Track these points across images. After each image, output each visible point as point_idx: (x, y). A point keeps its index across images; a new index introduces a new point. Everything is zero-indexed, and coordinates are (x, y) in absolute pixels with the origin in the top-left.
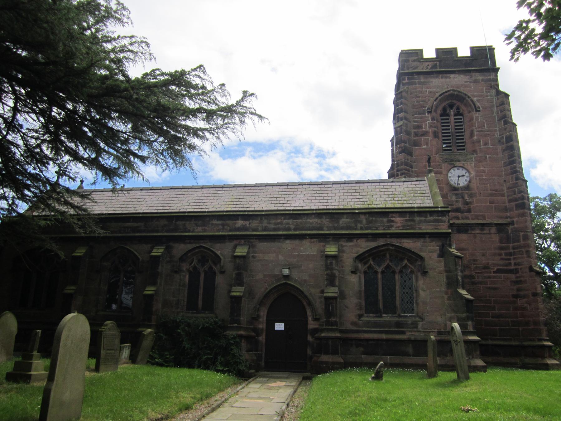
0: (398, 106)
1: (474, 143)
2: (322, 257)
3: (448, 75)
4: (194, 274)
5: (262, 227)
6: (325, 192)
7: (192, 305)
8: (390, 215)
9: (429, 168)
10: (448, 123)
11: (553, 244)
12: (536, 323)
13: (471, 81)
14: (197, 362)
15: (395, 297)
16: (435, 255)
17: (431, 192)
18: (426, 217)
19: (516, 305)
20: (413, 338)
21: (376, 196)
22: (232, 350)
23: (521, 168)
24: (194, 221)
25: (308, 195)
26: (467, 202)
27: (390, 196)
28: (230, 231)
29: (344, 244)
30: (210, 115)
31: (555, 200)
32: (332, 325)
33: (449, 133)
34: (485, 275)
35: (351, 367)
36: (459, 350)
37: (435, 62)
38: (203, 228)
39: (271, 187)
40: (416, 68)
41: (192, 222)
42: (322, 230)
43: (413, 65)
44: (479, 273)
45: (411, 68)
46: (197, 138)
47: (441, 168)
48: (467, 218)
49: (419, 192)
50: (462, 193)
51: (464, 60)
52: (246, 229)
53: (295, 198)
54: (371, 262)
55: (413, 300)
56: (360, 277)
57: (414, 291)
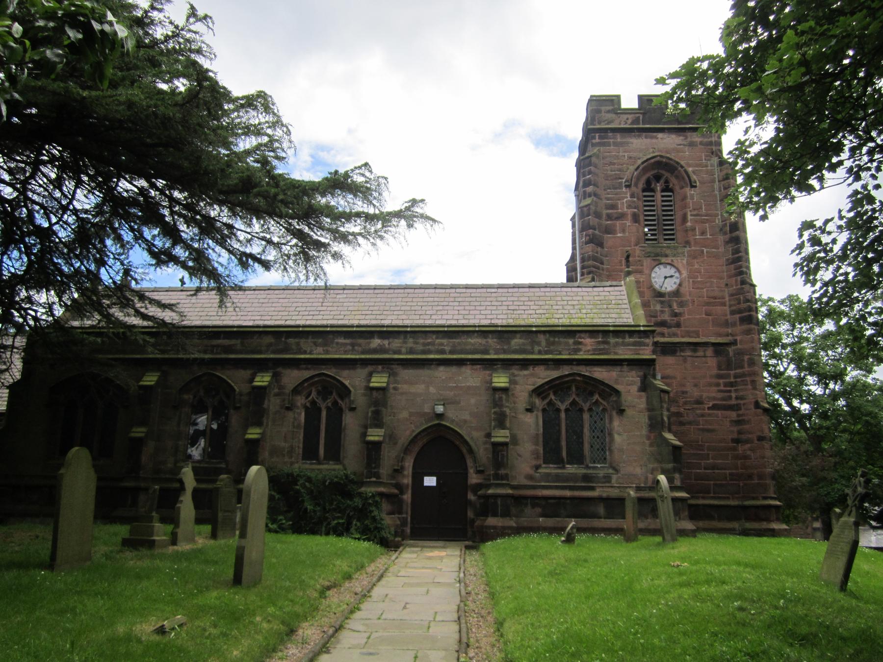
0: (584, 176)
1: (687, 231)
2: (487, 390)
3: (655, 134)
4: (313, 412)
5: (407, 348)
6: (488, 299)
7: (310, 453)
10: (653, 201)
12: (761, 477)
13: (685, 143)
14: (324, 529)
15: (582, 443)
16: (634, 389)
17: (630, 302)
18: (624, 338)
20: (605, 495)
21: (557, 307)
22: (371, 512)
23: (748, 268)
24: (313, 338)
25: (465, 304)
26: (676, 313)
27: (576, 307)
28: (363, 353)
29: (516, 372)
30: (369, 218)
33: (654, 215)
34: (698, 412)
35: (526, 533)
36: (665, 509)
37: (637, 115)
38: (325, 348)
39: (412, 291)
41: (309, 341)
42: (489, 354)
44: (689, 409)
45: (604, 121)
46: (345, 243)
47: (642, 265)
48: (675, 335)
49: (613, 302)
50: (669, 301)
52: (385, 351)
53: (447, 308)
55: (605, 447)
57: (607, 435)
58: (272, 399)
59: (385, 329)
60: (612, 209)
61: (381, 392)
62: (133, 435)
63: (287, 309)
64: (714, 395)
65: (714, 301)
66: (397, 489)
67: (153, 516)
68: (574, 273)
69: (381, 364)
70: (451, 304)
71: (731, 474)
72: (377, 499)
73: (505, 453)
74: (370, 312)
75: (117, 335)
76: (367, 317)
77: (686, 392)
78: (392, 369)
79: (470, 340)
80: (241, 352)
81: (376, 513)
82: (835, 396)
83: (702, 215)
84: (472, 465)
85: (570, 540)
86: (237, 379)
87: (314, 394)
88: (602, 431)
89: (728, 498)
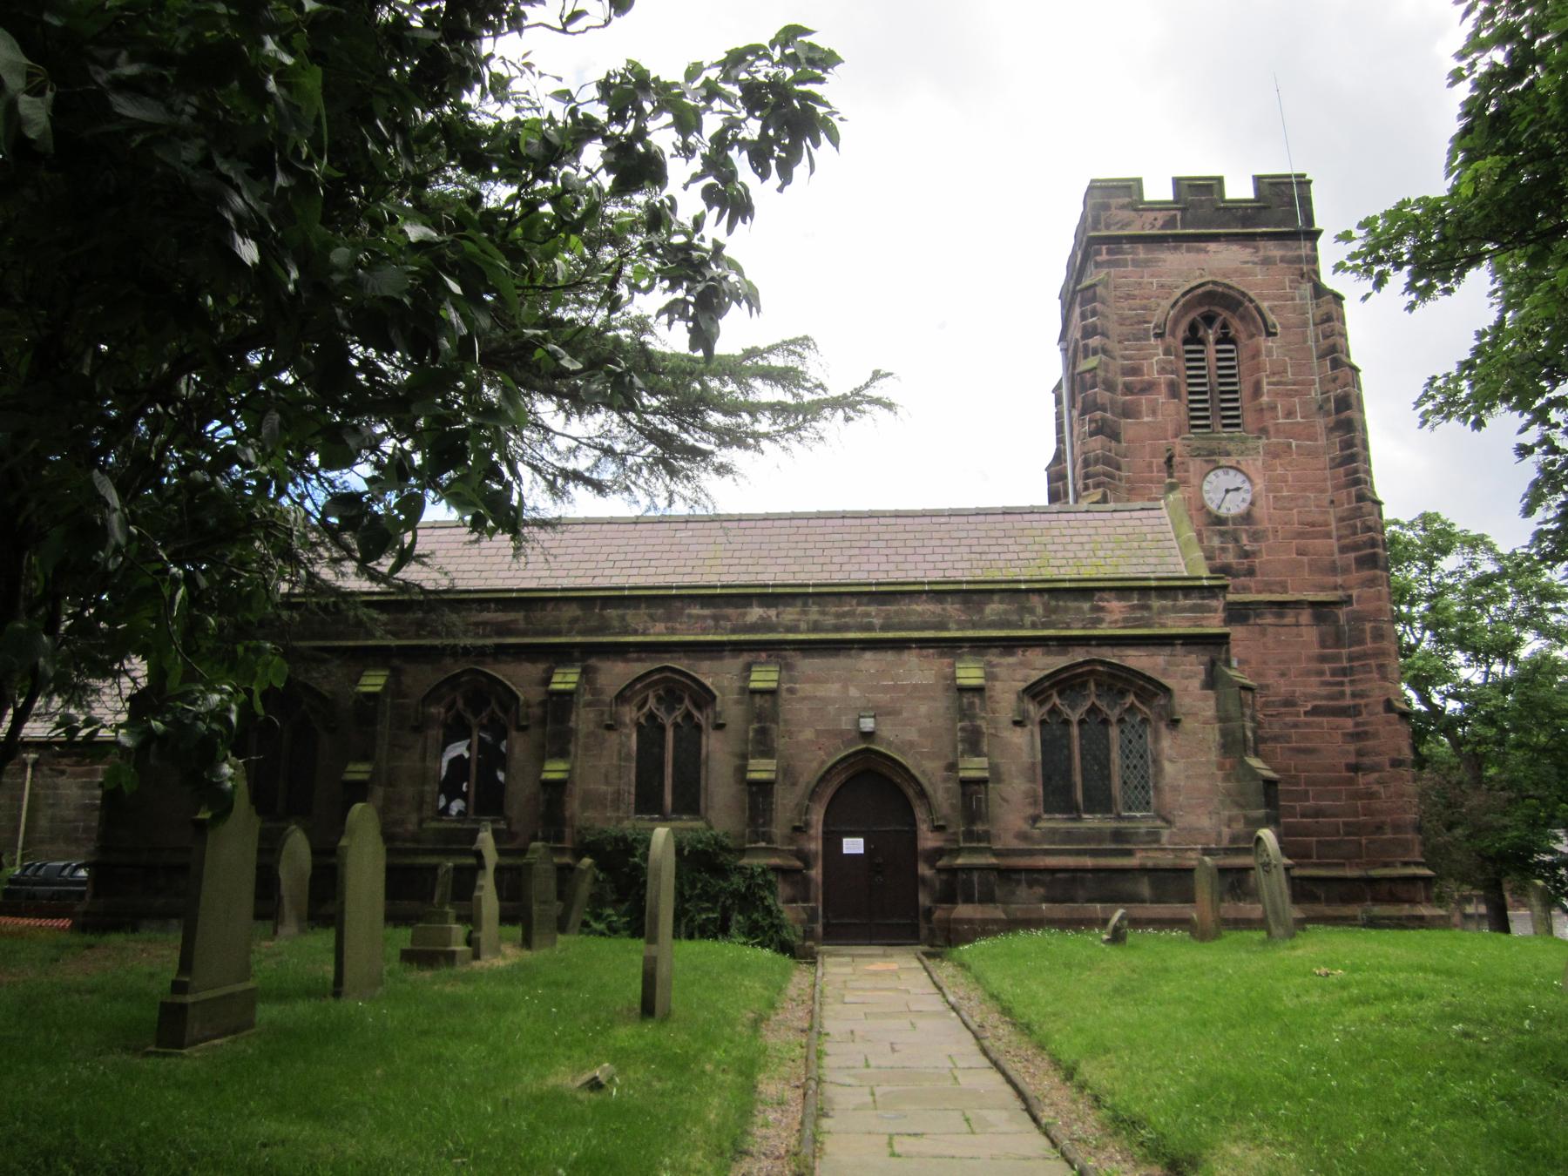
1: (1262, 410)
2: (947, 690)
3: (1203, 245)
4: (650, 732)
8: (1098, 595)
9: (1168, 481)
10: (1202, 360)
11: (1428, 633)
12: (1397, 828)
13: (1256, 259)
15: (1108, 777)
16: (1195, 684)
17: (1177, 537)
18: (1176, 599)
19: (1355, 787)
20: (1150, 864)
21: (1054, 547)
22: (763, 899)
23: (1368, 472)
24: (647, 607)
25: (895, 544)
26: (1246, 551)
27: (1087, 547)
28: (733, 631)
29: (995, 660)
31: (1436, 526)
32: (979, 841)
34: (1287, 719)
37: (1173, 212)
38: (669, 624)
40: (1127, 225)
42: (946, 628)
43: (1118, 218)
44: (1272, 716)
47: (1187, 471)
48: (1246, 589)
49: (1149, 537)
50: (1235, 530)
51: (1241, 208)
52: (772, 628)
54: (1056, 700)
55: (1147, 782)
56: (1032, 735)
58: (582, 712)
59: (770, 590)
60: (1133, 375)
61: (768, 697)
62: (349, 777)
63: (594, 557)
64: (1314, 690)
65: (1312, 529)
66: (799, 858)
67: (447, 913)
68: (1060, 483)
69: (765, 650)
70: (872, 544)
71: (1346, 824)
72: (771, 877)
73: (982, 796)
74: (737, 561)
75: (324, 608)
76: (732, 569)
77: (1267, 687)
78: (784, 658)
79: (914, 607)
80: (524, 634)
81: (770, 901)
82: (1505, 687)
83: (1285, 384)
84: (924, 817)
85: (1117, 937)
86: (521, 679)
87: (652, 703)
88: (1141, 757)
89: (1343, 865)
